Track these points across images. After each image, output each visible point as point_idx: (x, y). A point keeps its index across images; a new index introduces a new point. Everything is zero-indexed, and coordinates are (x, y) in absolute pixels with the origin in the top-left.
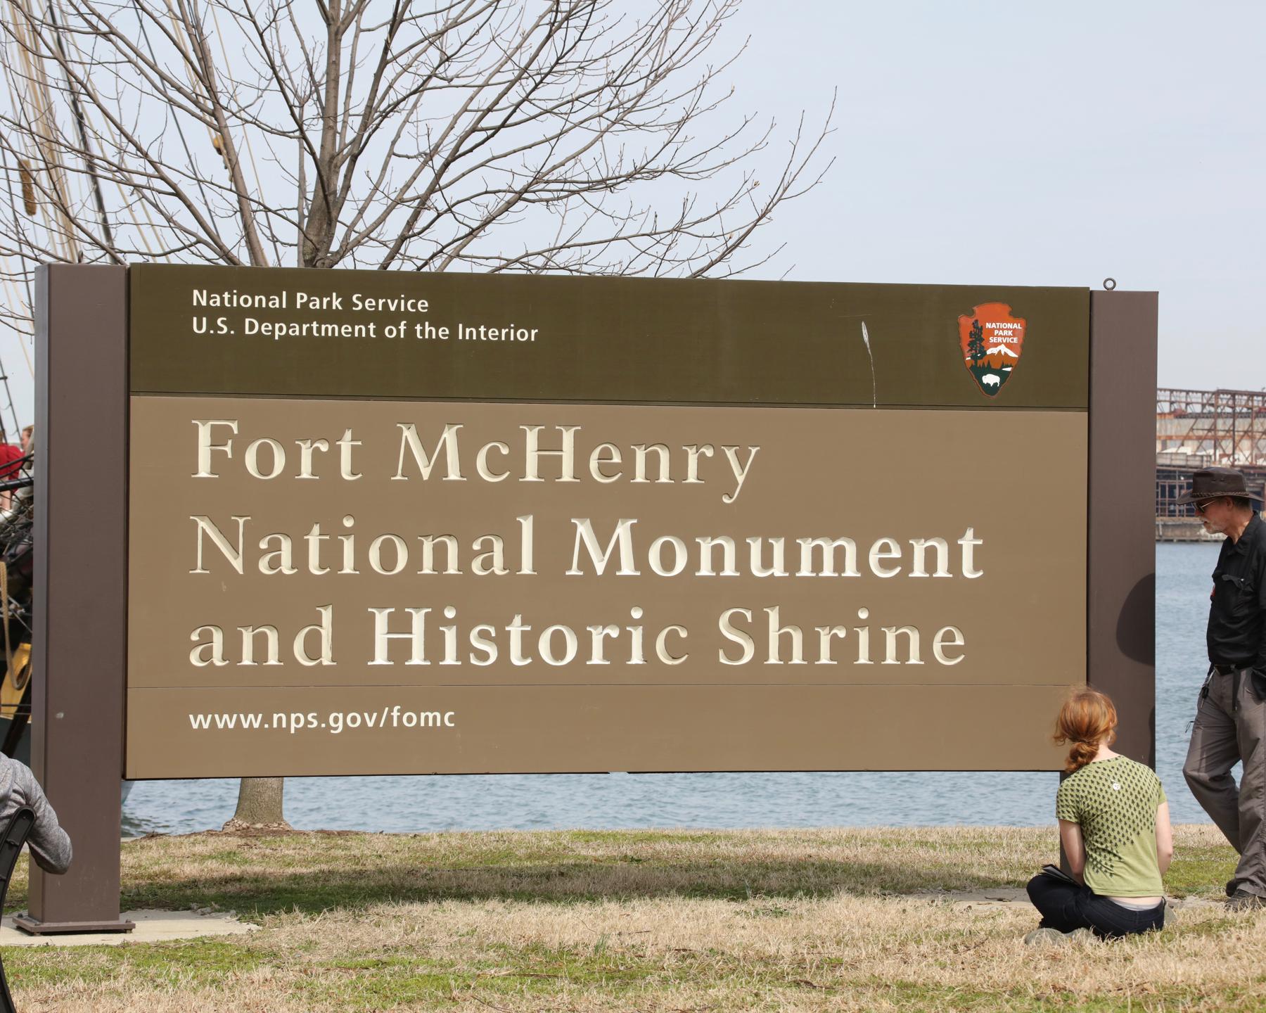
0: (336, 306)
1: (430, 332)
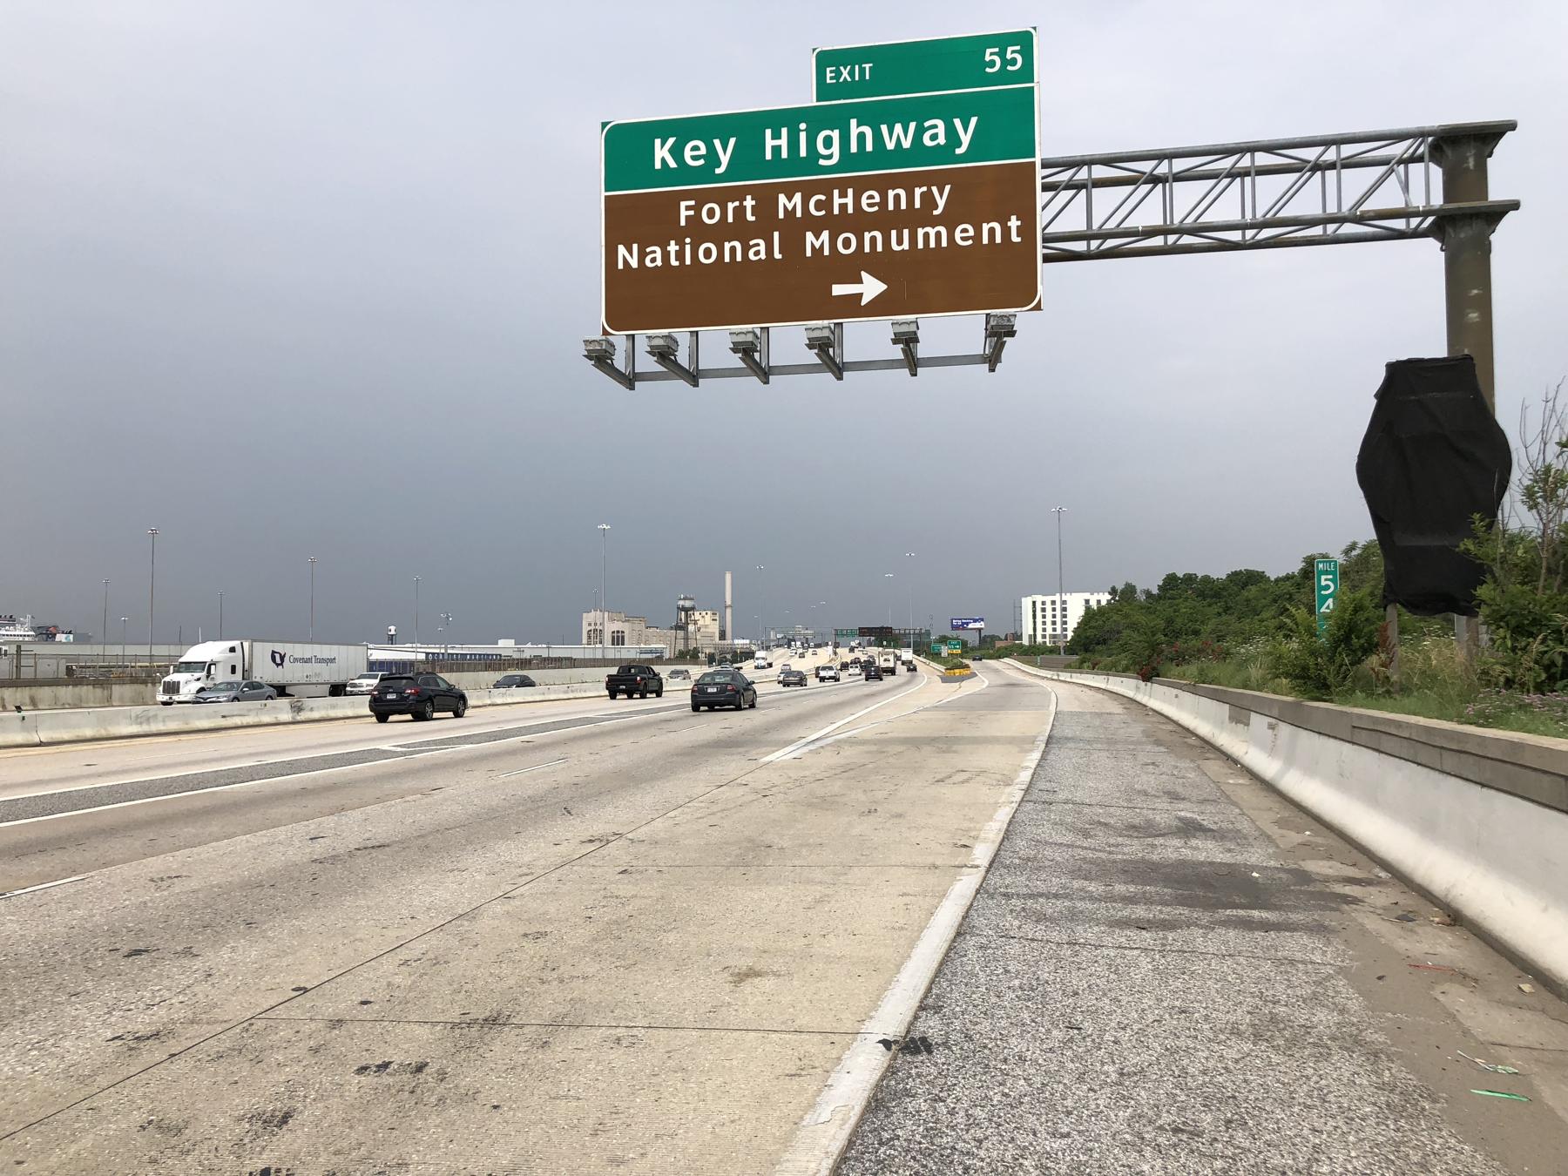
0: (663, 160)
1: (862, 137)
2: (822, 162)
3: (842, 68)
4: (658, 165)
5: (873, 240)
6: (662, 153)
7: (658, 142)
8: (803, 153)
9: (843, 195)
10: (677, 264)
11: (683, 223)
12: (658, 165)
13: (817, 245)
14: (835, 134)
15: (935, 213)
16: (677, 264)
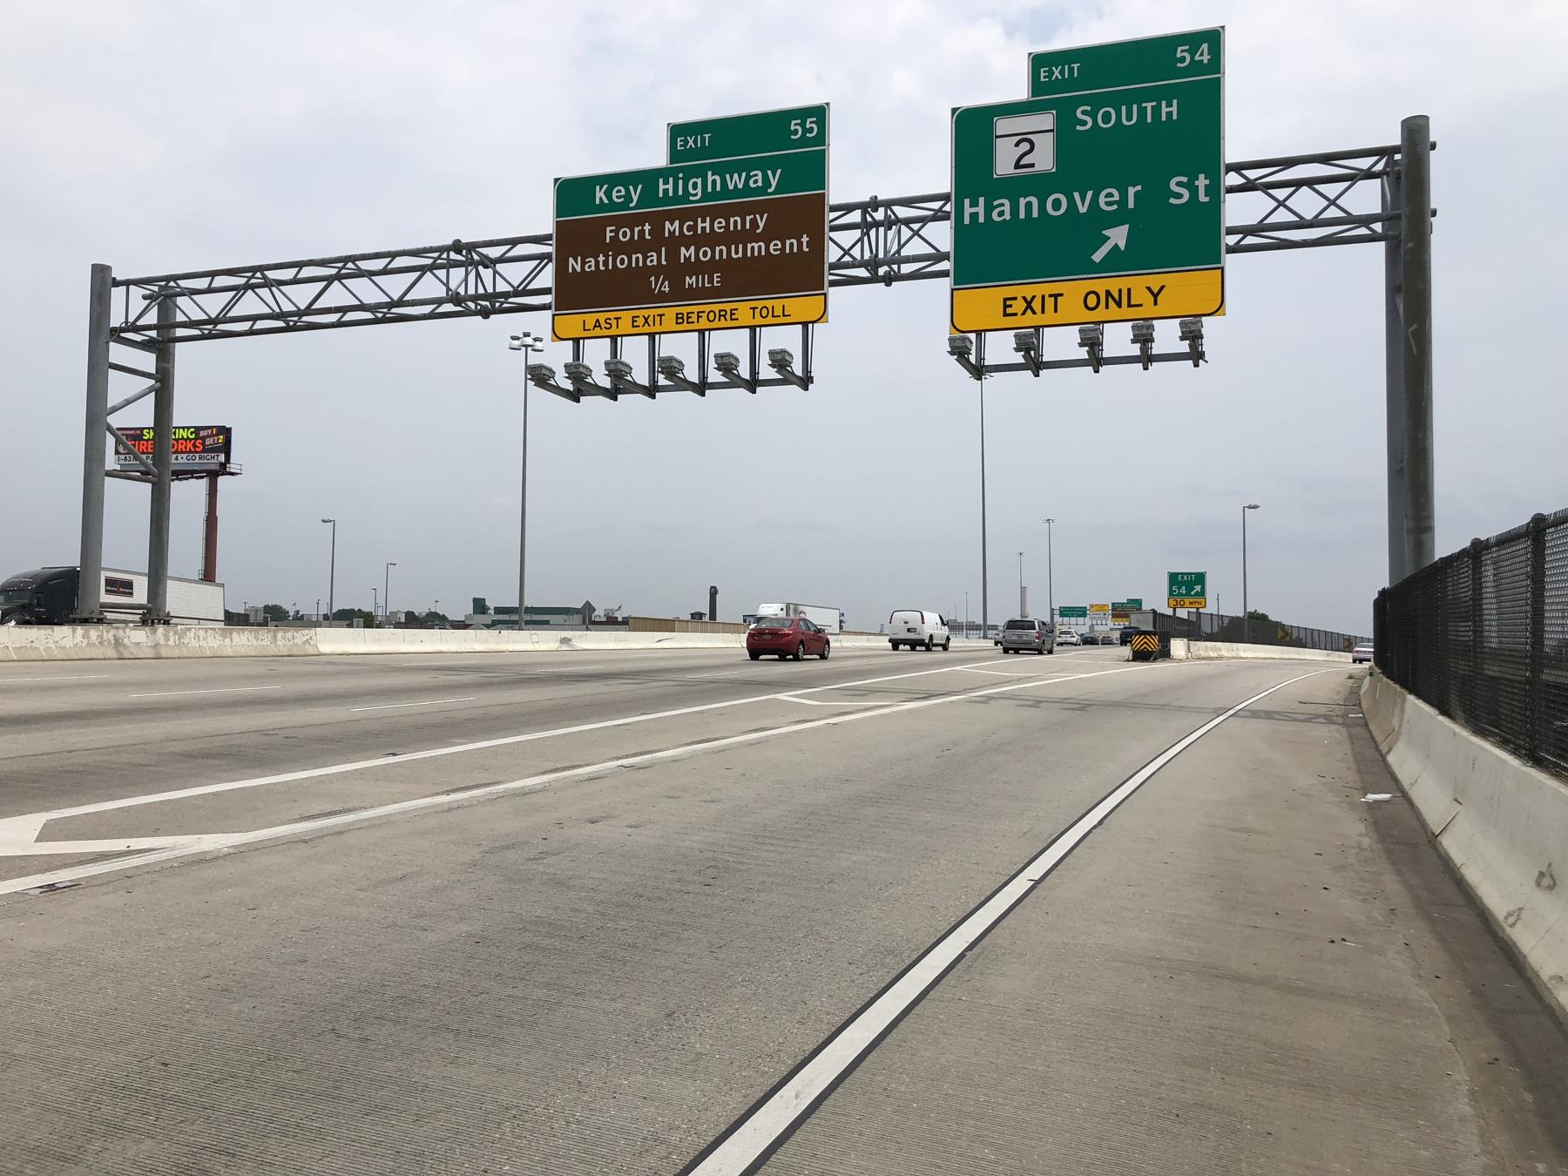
0: (601, 198)
1: (714, 182)
2: (691, 198)
3: (688, 138)
4: (598, 202)
5: (1029, 205)
6: (600, 194)
7: (598, 187)
8: (680, 193)
9: (704, 221)
10: (604, 268)
11: (608, 241)
12: (598, 202)
13: (687, 255)
14: (699, 181)
15: (758, 231)
16: (604, 268)
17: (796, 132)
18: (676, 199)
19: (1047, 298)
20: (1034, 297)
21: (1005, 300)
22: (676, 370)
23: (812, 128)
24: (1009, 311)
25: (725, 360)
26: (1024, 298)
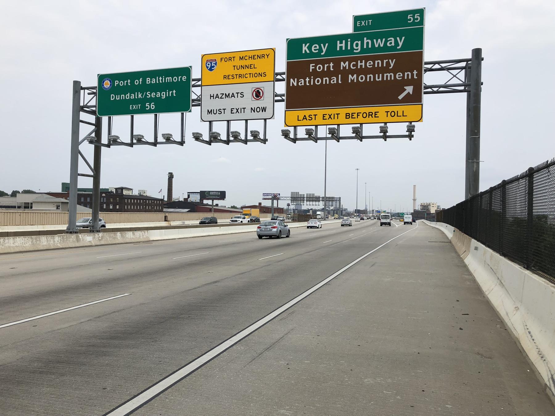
0: (305, 50)
1: (368, 43)
2: (355, 51)
4: (304, 52)
6: (305, 48)
7: (304, 45)
8: (349, 48)
12: (304, 52)
15: (390, 68)
17: (410, 20)
18: (347, 52)
19: (335, 114)
20: (331, 114)
21: (323, 115)
22: (238, 136)
23: (411, 19)
24: (324, 118)
25: (234, 134)
26: (329, 114)
